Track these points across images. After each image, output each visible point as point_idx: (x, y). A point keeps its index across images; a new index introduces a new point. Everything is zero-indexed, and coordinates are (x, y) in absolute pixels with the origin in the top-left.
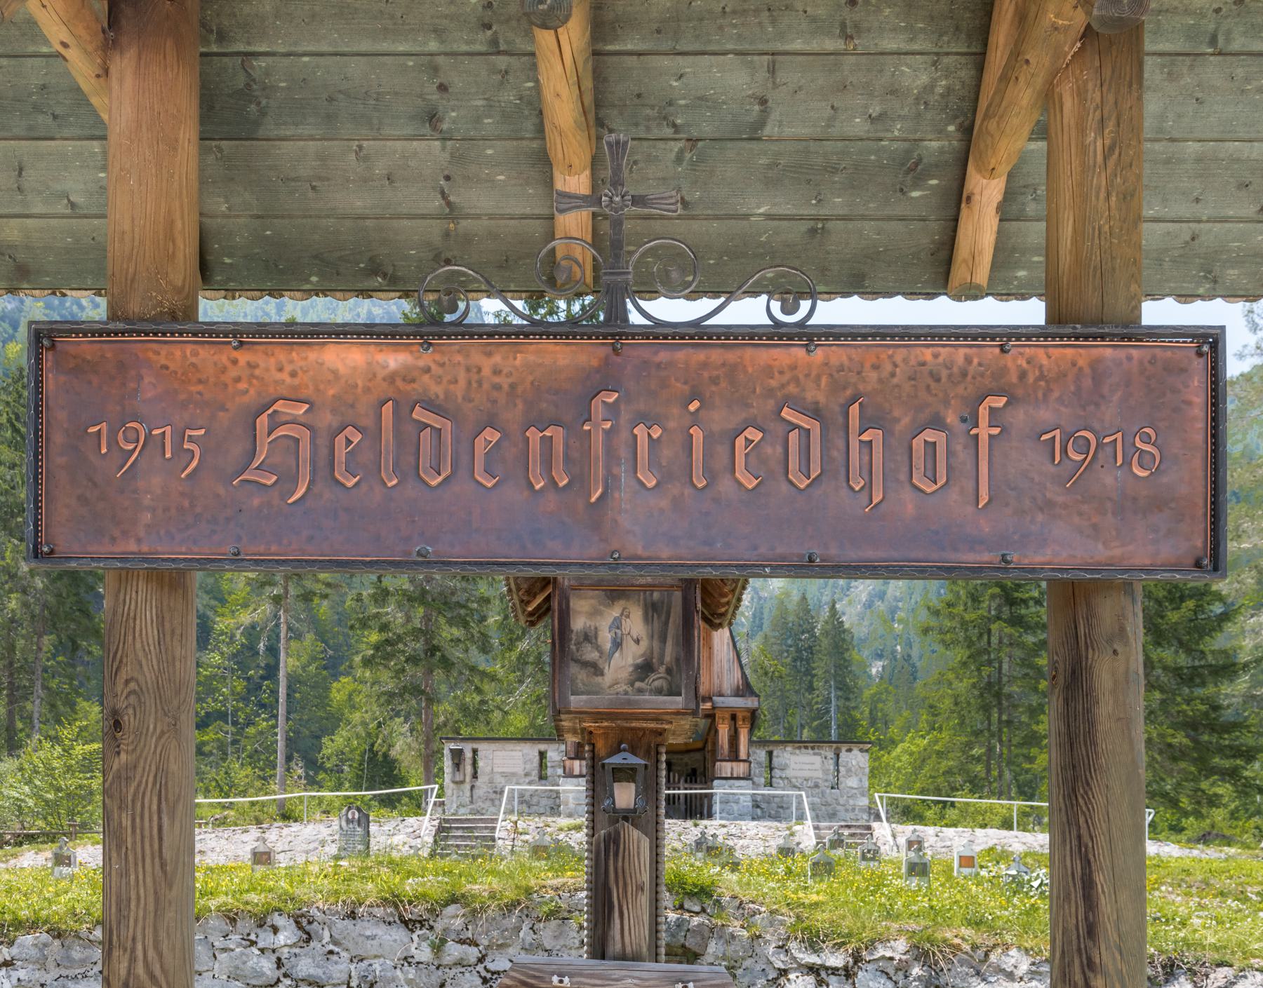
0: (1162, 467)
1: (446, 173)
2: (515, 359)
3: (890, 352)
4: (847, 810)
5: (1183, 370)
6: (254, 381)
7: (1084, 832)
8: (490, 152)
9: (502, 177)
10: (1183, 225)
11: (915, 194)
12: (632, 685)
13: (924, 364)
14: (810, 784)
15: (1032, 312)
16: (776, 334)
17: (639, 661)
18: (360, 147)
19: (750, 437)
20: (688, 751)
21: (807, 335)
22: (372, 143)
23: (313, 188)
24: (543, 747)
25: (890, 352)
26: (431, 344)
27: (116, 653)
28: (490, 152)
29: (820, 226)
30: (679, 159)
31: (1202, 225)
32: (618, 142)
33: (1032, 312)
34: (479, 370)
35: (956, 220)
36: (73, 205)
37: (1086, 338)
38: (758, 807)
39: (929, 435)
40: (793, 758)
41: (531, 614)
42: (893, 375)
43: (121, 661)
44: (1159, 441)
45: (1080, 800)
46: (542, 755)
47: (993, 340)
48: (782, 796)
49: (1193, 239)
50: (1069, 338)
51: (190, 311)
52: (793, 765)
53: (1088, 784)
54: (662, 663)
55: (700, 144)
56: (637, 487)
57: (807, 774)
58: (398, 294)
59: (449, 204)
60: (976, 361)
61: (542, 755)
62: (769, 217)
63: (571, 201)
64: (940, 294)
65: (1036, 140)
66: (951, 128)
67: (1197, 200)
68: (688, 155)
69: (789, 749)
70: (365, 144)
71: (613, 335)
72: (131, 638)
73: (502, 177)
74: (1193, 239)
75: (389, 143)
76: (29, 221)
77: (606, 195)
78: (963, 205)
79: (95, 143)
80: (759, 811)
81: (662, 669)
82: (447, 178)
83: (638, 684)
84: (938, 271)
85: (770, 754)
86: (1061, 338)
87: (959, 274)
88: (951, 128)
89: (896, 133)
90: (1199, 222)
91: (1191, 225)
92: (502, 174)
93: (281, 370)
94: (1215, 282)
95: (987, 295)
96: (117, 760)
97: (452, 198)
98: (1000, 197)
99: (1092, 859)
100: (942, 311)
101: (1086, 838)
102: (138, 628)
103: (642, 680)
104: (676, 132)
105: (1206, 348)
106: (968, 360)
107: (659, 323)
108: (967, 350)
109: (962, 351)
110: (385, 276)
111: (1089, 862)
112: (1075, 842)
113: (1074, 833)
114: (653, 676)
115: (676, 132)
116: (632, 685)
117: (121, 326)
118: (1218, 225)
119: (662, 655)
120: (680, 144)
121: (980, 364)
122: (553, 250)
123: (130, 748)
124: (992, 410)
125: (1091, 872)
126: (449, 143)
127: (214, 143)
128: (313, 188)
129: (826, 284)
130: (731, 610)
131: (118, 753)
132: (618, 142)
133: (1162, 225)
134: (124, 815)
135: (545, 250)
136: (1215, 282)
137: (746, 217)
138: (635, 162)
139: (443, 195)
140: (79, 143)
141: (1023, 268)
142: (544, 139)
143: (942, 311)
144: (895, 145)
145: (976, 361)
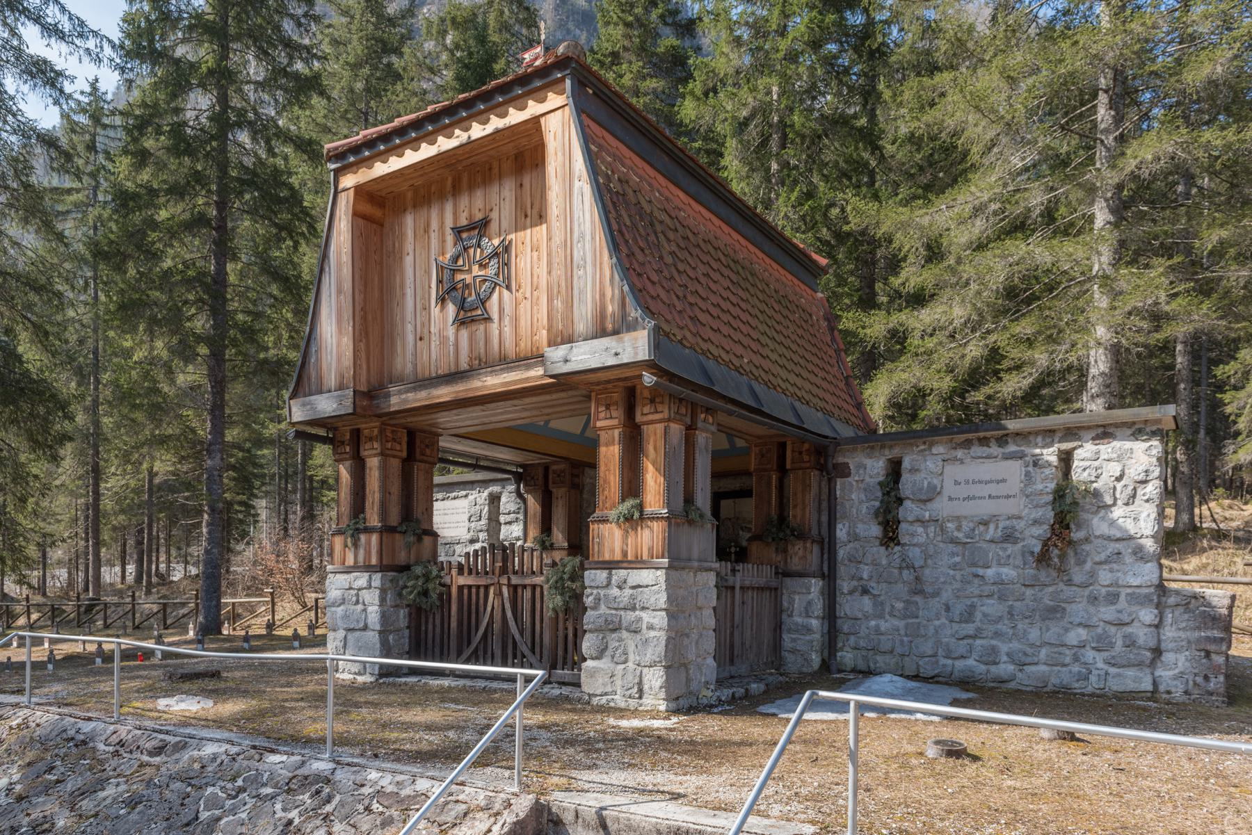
4: (1093, 600)
14: (991, 532)
40: (952, 471)
52: (949, 489)
57: (985, 508)
69: (939, 449)
85: (895, 470)
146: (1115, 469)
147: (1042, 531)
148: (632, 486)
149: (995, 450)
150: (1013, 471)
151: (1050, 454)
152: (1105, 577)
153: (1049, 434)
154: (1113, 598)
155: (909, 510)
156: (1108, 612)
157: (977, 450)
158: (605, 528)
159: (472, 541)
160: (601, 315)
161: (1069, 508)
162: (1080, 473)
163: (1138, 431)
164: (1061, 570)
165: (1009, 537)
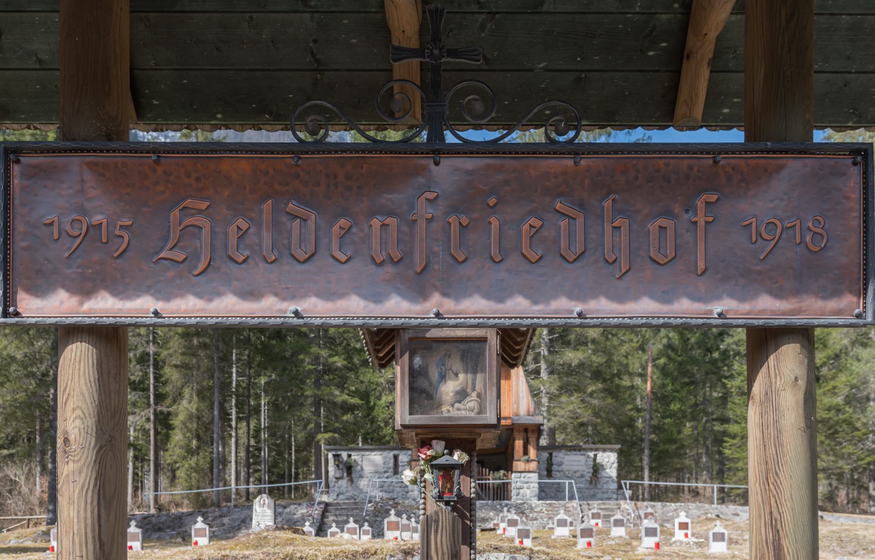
0: (829, 244)
1: (314, 37)
2: (362, 167)
3: (634, 162)
4: (603, 493)
5: (844, 174)
6: (169, 185)
7: (774, 510)
8: (345, 22)
9: (354, 41)
10: (839, 75)
11: (651, 53)
12: (453, 406)
13: (658, 171)
14: (577, 475)
15: (736, 136)
16: (550, 149)
17: (458, 388)
18: (251, 18)
19: (533, 224)
20: (495, 454)
21: (576, 150)
22: (259, 14)
23: (217, 49)
24: (396, 452)
25: (634, 162)
26: (300, 158)
27: (66, 388)
28: (345, 22)
29: (583, 76)
30: (482, 27)
31: (852, 76)
32: (437, 10)
33: (736, 136)
34: (336, 176)
35: (679, 72)
36: (40, 61)
37: (774, 152)
38: (543, 491)
39: (663, 222)
40: (567, 457)
41: (382, 359)
42: (636, 178)
43: (69, 395)
44: (826, 226)
45: (771, 486)
46: (396, 457)
47: (708, 153)
48: (559, 483)
49: (845, 86)
50: (762, 152)
51: (122, 134)
52: (566, 462)
53: (777, 475)
54: (474, 389)
55: (498, 16)
56: (452, 261)
57: (576, 468)
58: (281, 127)
59: (317, 61)
60: (695, 169)
61: (396, 457)
62: (546, 70)
63: (402, 53)
64: (669, 126)
65: (736, 14)
66: (676, 6)
67: (849, 58)
68: (489, 25)
69: (563, 451)
70: (255, 15)
71: (433, 152)
72: (77, 377)
73: (354, 41)
74: (845, 86)
75: (272, 15)
76: (7, 73)
77: (428, 49)
78: (685, 61)
79: (55, 14)
80: (543, 494)
81: (474, 394)
82: (315, 41)
83: (457, 405)
84: (666, 113)
85: (551, 454)
86: (757, 152)
87: (681, 109)
88: (676, 6)
89: (637, 9)
90: (850, 73)
91: (844, 75)
92: (355, 38)
93: (188, 176)
94: (861, 117)
95: (702, 127)
96: (66, 467)
97: (318, 56)
98: (711, 56)
99: (780, 529)
100: (672, 136)
101: (776, 514)
102: (82, 369)
103: (460, 402)
104: (479, 8)
105: (859, 158)
106: (690, 167)
107: (466, 142)
108: (690, 162)
109: (686, 162)
110: (270, 114)
111: (778, 531)
112: (768, 517)
113: (767, 511)
114: (468, 399)
115: (479, 8)
116: (453, 406)
117: (69, 144)
118: (864, 75)
119: (474, 385)
120: (483, 16)
121: (698, 171)
122: (392, 88)
123: (76, 459)
124: (708, 204)
125: (779, 539)
126: (316, 15)
127: (143, 15)
128: (217, 49)
129: (588, 120)
130: (523, 356)
131: (68, 463)
132: (437, 10)
133: (824, 75)
134: (71, 509)
135: (385, 89)
136: (861, 117)
137: (531, 70)
138: (451, 30)
139: (313, 55)
140: (43, 14)
141: (727, 107)
142: (384, 12)
143: (672, 136)
144: (637, 17)
145: (695, 169)
146: (607, 460)
147: (590, 475)
148: (526, 452)
149: (578, 453)
150: (583, 458)
151: (591, 454)
152: (605, 486)
153: (591, 450)
154: (607, 492)
155: (555, 467)
156: (606, 496)
157: (573, 452)
158: (519, 463)
159: (385, 472)
160: (529, 411)
161: (597, 469)
162: (598, 460)
163: (612, 450)
164: (596, 485)
165: (582, 476)
